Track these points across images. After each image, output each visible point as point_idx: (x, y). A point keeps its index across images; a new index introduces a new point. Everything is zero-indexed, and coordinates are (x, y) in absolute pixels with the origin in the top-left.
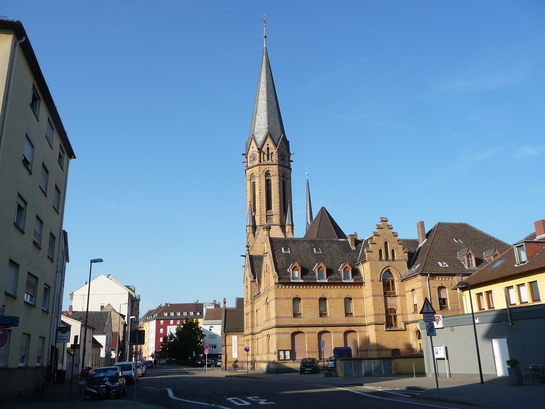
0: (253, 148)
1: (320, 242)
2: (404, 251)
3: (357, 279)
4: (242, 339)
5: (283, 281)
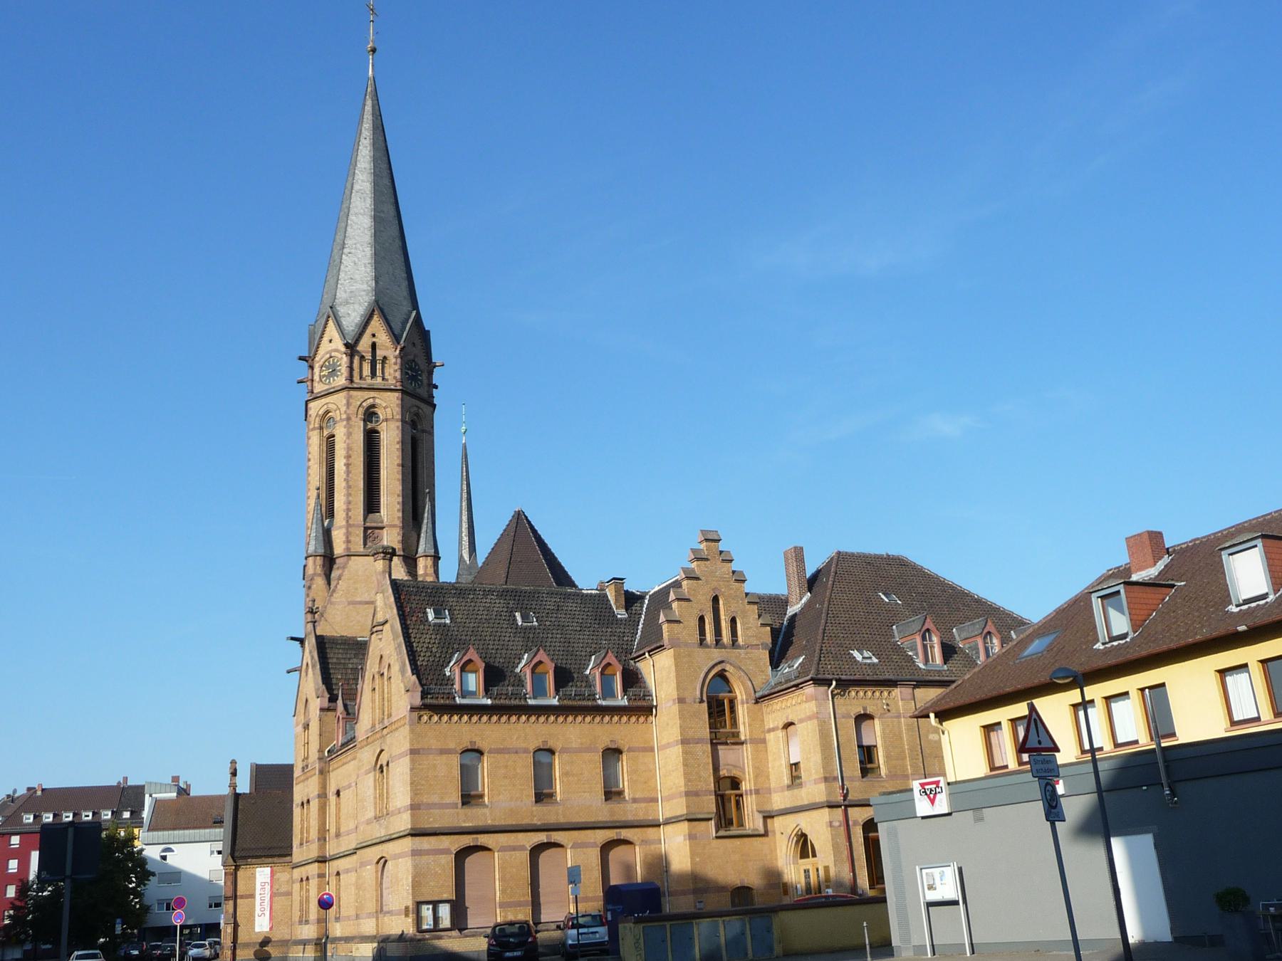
0: (330, 341)
1: (532, 595)
2: (760, 621)
3: (637, 697)
4: (283, 876)
5: (434, 702)
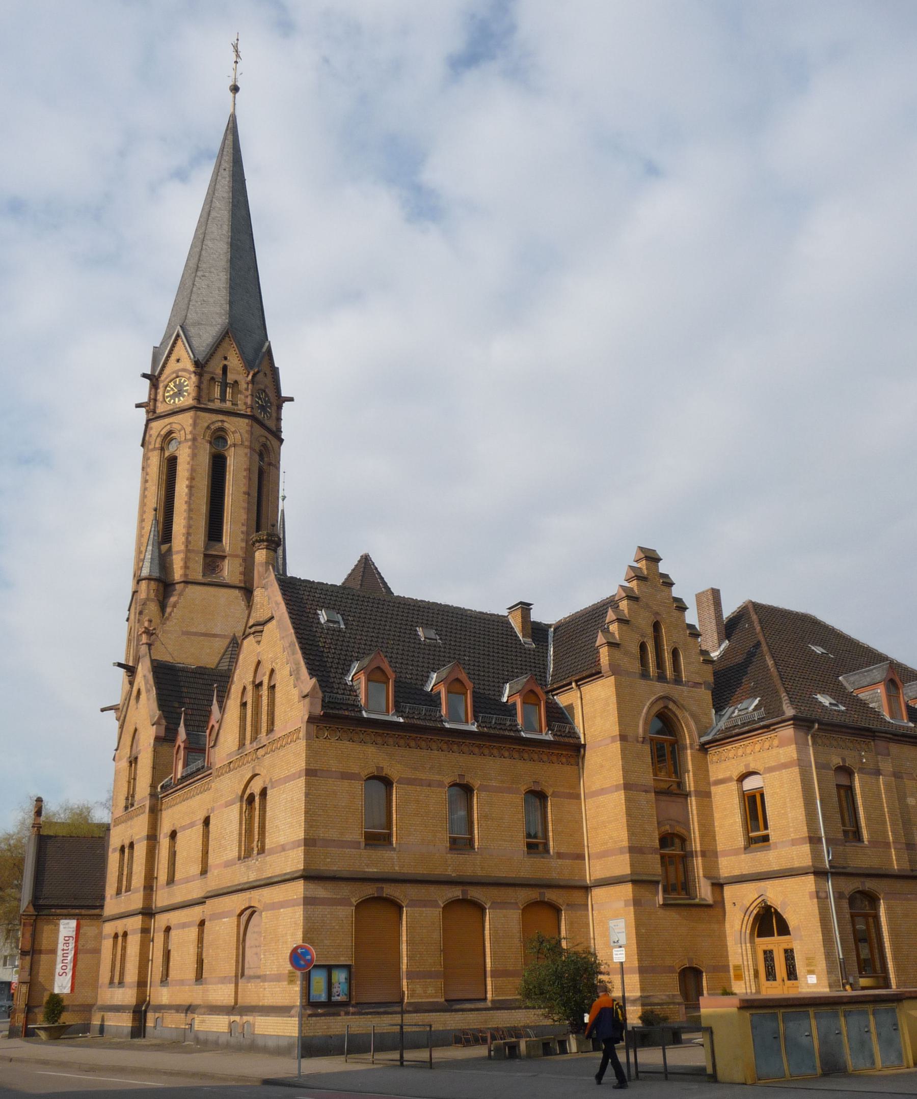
0: (178, 361)
